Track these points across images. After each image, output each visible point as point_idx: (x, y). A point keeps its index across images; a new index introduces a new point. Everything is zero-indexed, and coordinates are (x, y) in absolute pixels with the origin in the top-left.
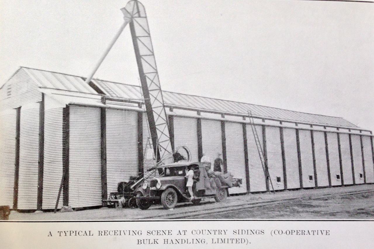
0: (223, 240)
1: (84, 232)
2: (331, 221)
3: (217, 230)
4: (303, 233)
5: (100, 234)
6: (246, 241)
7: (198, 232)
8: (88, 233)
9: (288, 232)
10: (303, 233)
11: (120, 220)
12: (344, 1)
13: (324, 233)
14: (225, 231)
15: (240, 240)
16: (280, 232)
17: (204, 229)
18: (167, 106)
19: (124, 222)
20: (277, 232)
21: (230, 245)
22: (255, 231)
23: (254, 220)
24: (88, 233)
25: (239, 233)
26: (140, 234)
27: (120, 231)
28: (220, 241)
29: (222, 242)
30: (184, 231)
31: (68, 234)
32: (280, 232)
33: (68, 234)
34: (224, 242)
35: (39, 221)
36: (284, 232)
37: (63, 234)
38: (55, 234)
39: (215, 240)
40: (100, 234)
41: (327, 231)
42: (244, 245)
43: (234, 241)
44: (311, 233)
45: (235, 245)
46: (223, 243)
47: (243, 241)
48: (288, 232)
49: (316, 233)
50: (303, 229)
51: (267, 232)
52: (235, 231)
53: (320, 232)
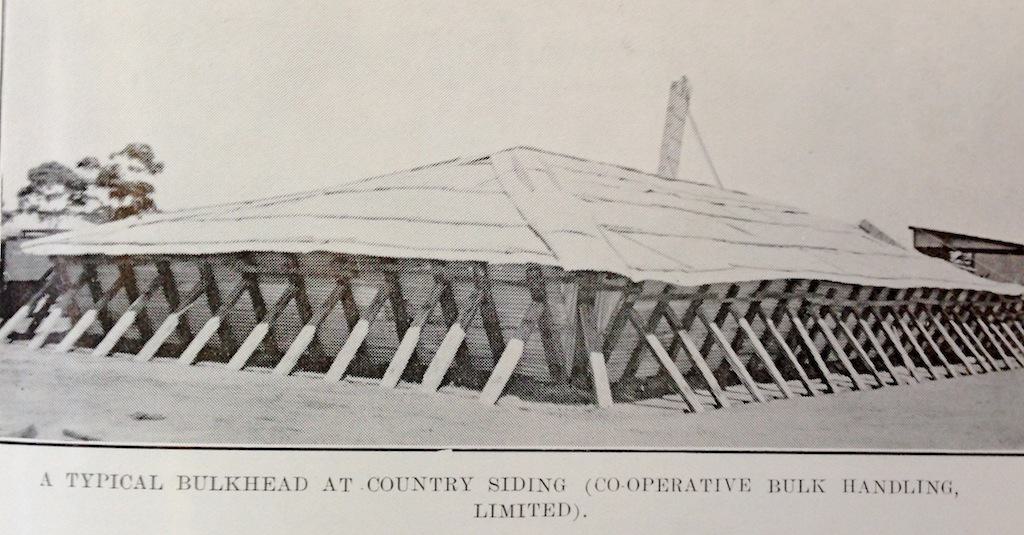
0: (508, 508)
1: (136, 479)
2: (1005, 458)
3: (77, 474)
4: (676, 485)
5: (451, 487)
6: (573, 509)
7: (387, 484)
8: (148, 482)
9: (633, 484)
10: (676, 485)
11: (870, 450)
12: (3, 31)
13: (736, 486)
14: (467, 481)
15: (557, 506)
16: (613, 484)
17: (403, 476)
18: (21, 203)
19: (1001, 458)
20: (602, 485)
21: (528, 524)
22: (552, 482)
23: (476, 450)
24: (148, 482)
25: (213, 481)
26: (559, 487)
27: (153, 477)
28: (498, 510)
29: (504, 515)
30: (343, 481)
31: (93, 481)
32: (613, 484)
33: (93, 481)
34: (509, 515)
35: (421, 447)
36: (623, 483)
37: (79, 482)
38: (60, 481)
39: (485, 509)
40: (451, 487)
41: (266, 478)
42: (564, 524)
43: (540, 512)
44: (700, 487)
45: (538, 524)
46: (509, 519)
47: (565, 509)
48: (633, 484)
49: (712, 487)
50: (451, 475)
51: (833, 486)
52: (494, 481)
53: (723, 483)
